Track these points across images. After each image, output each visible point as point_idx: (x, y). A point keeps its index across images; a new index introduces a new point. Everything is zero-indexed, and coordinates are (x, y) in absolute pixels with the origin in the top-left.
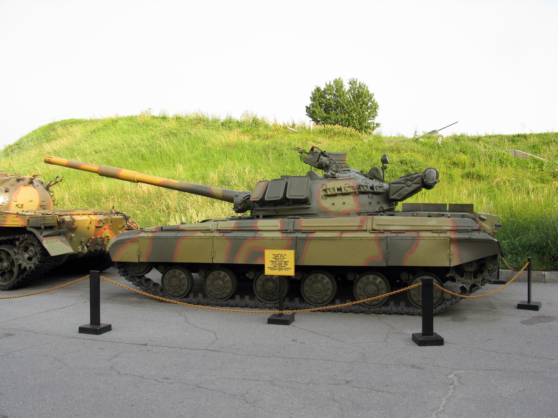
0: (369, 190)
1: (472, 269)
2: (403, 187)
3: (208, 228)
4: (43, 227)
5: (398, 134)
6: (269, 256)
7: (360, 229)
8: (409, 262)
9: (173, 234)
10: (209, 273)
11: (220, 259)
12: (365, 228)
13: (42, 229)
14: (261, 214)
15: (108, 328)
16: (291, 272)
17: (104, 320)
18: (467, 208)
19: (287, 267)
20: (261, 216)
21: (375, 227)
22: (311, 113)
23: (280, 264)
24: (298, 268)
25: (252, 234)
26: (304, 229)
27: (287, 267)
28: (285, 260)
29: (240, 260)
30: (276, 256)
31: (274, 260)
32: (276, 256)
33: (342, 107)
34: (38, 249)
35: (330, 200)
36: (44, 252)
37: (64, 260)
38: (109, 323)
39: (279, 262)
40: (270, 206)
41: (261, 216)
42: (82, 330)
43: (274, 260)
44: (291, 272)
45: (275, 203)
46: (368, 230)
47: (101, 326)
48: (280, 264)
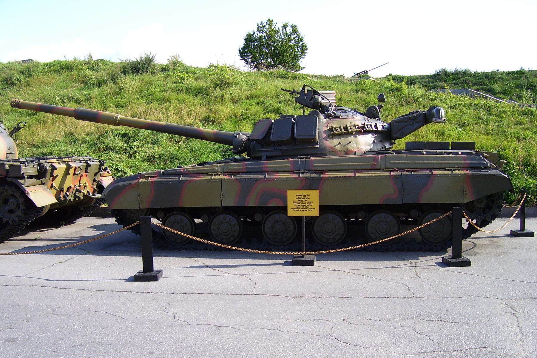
0: (374, 128)
1: (482, 205)
2: (406, 125)
3: (214, 171)
4: (26, 177)
5: (75, 59)
6: (292, 196)
7: (373, 167)
8: (423, 200)
9: (175, 179)
10: (214, 218)
11: (230, 202)
12: (378, 167)
13: (26, 178)
14: (264, 155)
15: (532, 234)
16: (315, 213)
17: (156, 267)
18: (471, 146)
19: (310, 207)
20: (264, 157)
21: (388, 166)
22: (243, 54)
23: (303, 205)
24: (322, 209)
25: (261, 176)
26: (315, 168)
27: (310, 207)
28: (308, 201)
29: (252, 202)
30: (299, 197)
31: (297, 200)
32: (299, 197)
33: (271, 49)
34: (21, 200)
35: (336, 141)
36: (30, 203)
37: (45, 211)
38: (533, 231)
39: (304, 204)
40: (274, 146)
41: (264, 157)
42: (137, 278)
43: (297, 200)
44: (315, 213)
45: (281, 143)
46: (381, 168)
47: (525, 232)
48: (303, 205)
